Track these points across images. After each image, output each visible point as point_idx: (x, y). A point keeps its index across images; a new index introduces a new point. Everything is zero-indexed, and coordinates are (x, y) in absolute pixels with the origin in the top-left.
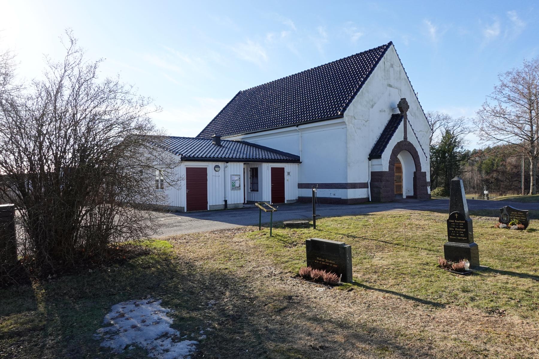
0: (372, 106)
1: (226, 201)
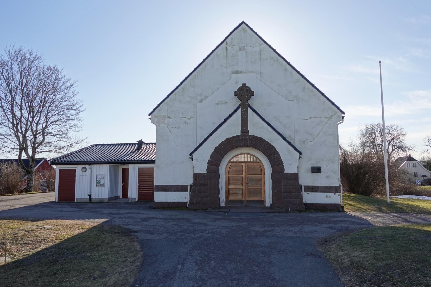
0: (201, 101)
1: (90, 196)
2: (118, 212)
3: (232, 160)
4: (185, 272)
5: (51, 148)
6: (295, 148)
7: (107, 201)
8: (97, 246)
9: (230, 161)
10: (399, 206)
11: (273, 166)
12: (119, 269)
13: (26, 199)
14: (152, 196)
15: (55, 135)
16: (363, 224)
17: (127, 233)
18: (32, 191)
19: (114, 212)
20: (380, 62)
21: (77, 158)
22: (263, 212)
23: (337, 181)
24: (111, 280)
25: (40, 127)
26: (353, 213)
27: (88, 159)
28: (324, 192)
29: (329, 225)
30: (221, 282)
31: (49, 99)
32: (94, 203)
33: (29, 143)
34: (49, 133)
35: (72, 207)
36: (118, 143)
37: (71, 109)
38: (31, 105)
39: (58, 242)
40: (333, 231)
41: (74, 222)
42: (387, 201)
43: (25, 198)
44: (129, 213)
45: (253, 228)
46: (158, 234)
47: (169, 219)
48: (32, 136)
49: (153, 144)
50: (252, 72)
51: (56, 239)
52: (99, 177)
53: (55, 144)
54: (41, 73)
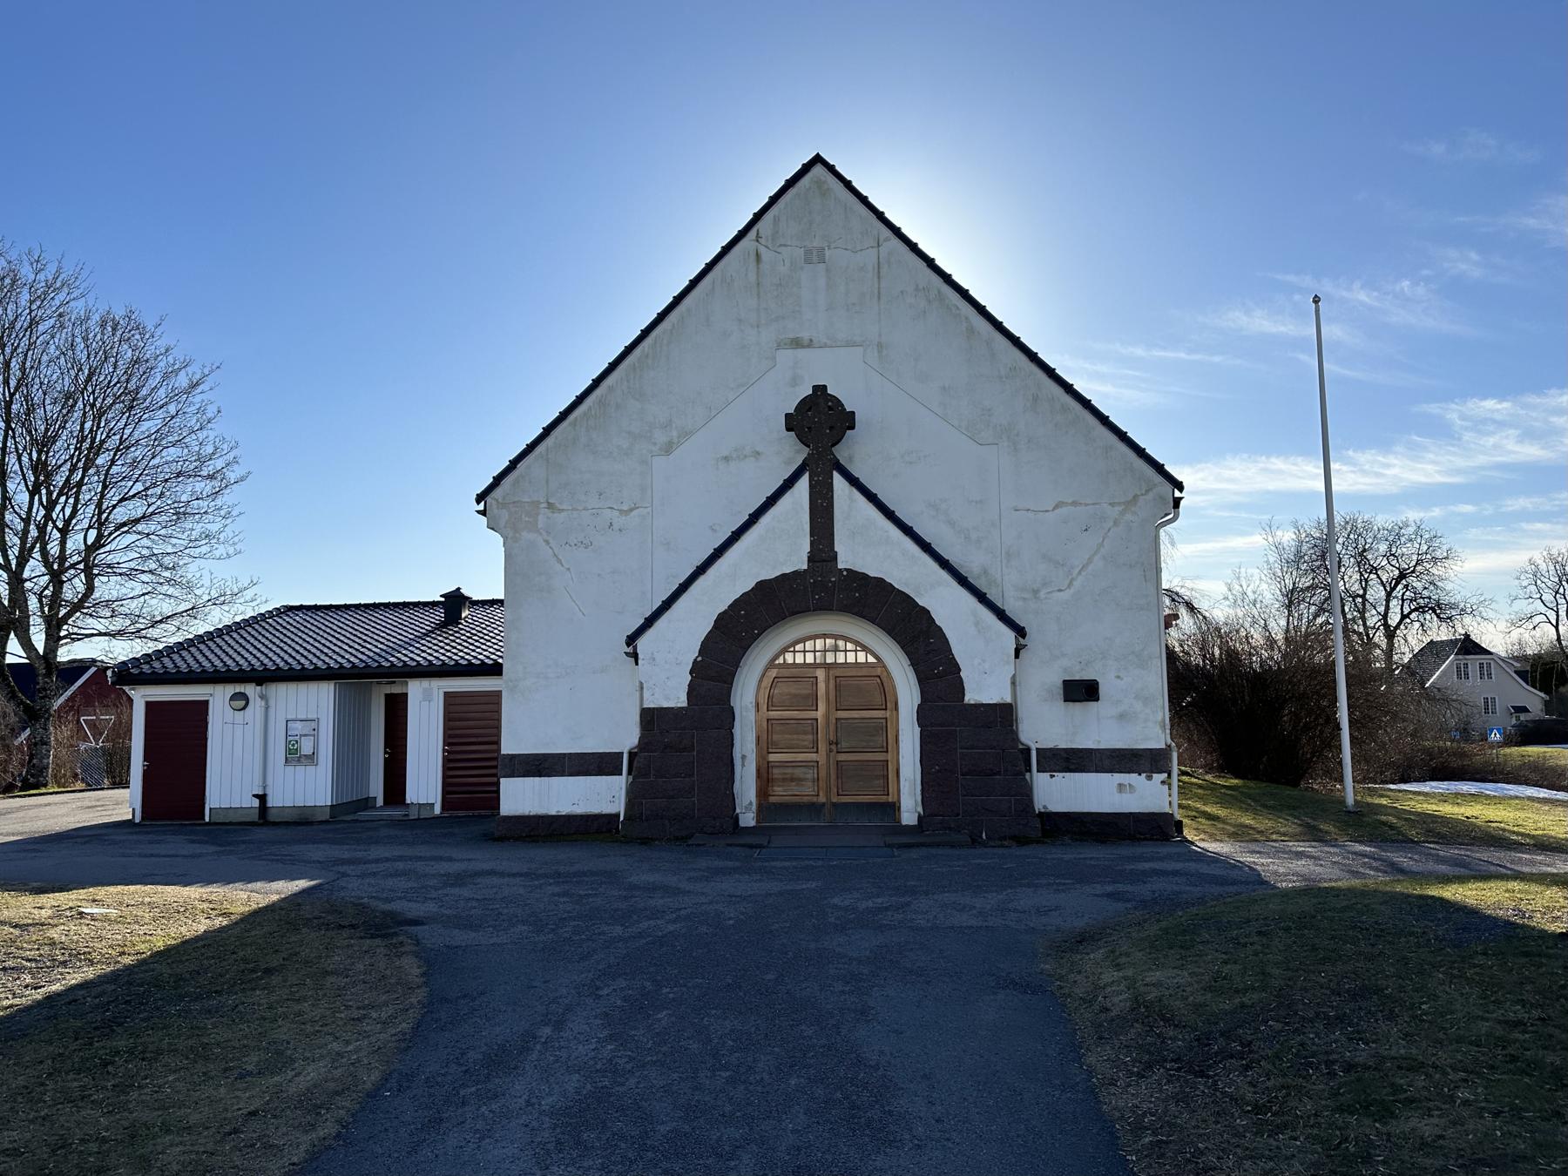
0: (668, 449)
1: (262, 798)
2: (359, 854)
3: (781, 660)
4: (560, 1048)
5: (118, 624)
6: (1002, 615)
7: (326, 816)
8: (268, 971)
9: (771, 664)
10: (1384, 818)
11: (922, 680)
12: (336, 1046)
13: (21, 814)
14: (492, 799)
15: (130, 575)
16: (1234, 883)
17: (383, 927)
18: (45, 785)
19: (346, 856)
20: (1316, 300)
21: (212, 660)
22: (889, 846)
23: (1158, 730)
24: (301, 1078)
25: (75, 543)
26: (1213, 847)
27: (254, 661)
28: (1111, 771)
29: (1109, 889)
30: (675, 1076)
31: (108, 437)
32: (275, 824)
33: (33, 603)
34: (109, 566)
35: (193, 842)
36: (342, 603)
37: (195, 474)
38: (39, 458)
39: (127, 960)
40: (1120, 906)
41: (193, 892)
42: (1343, 802)
43: (21, 808)
44: (401, 858)
45: (836, 901)
46: (494, 927)
47: (546, 876)
48: (47, 578)
49: (493, 602)
50: (850, 344)
51: (123, 953)
52: (298, 728)
53: (133, 606)
54: (78, 340)
